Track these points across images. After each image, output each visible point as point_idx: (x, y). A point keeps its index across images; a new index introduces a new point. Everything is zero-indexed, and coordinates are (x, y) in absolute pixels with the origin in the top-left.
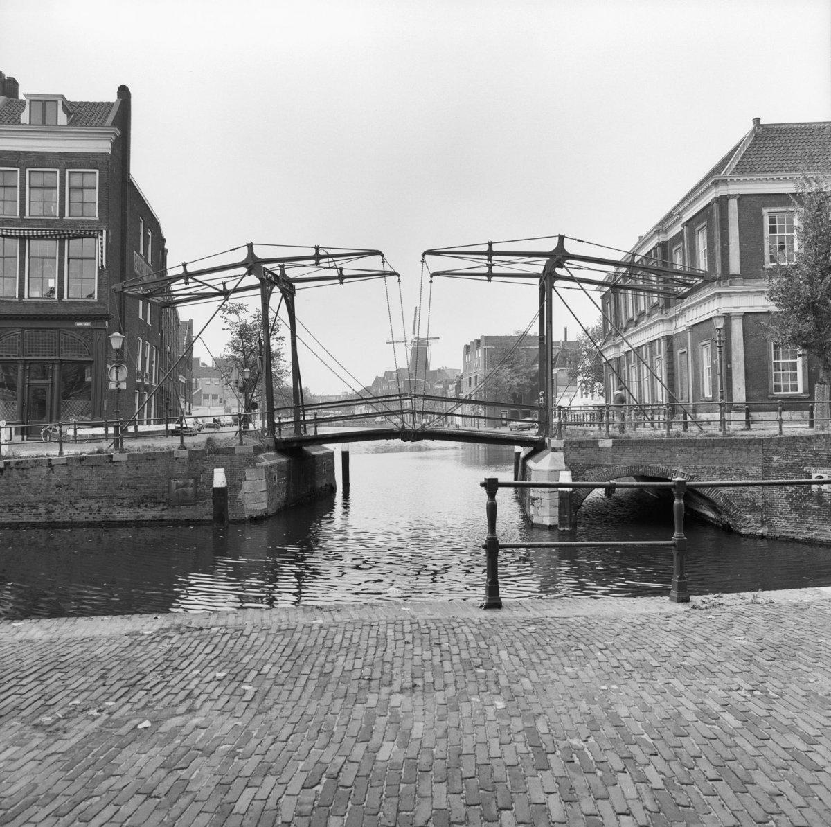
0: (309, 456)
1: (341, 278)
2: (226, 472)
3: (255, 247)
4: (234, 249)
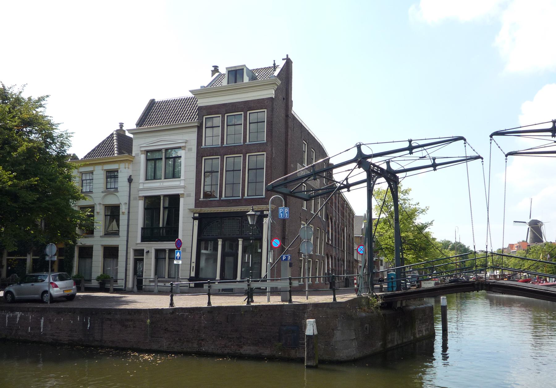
0: (412, 311)
1: (434, 166)
2: (317, 322)
3: (362, 147)
4: (347, 150)
